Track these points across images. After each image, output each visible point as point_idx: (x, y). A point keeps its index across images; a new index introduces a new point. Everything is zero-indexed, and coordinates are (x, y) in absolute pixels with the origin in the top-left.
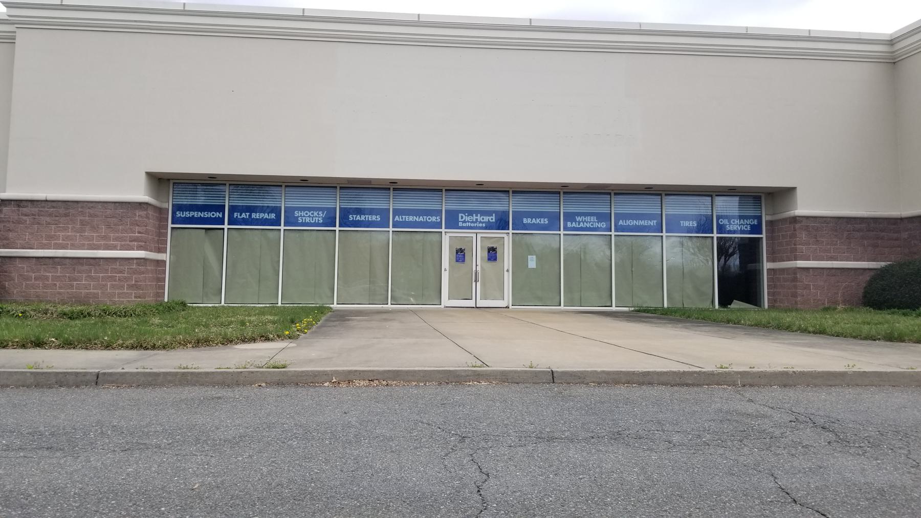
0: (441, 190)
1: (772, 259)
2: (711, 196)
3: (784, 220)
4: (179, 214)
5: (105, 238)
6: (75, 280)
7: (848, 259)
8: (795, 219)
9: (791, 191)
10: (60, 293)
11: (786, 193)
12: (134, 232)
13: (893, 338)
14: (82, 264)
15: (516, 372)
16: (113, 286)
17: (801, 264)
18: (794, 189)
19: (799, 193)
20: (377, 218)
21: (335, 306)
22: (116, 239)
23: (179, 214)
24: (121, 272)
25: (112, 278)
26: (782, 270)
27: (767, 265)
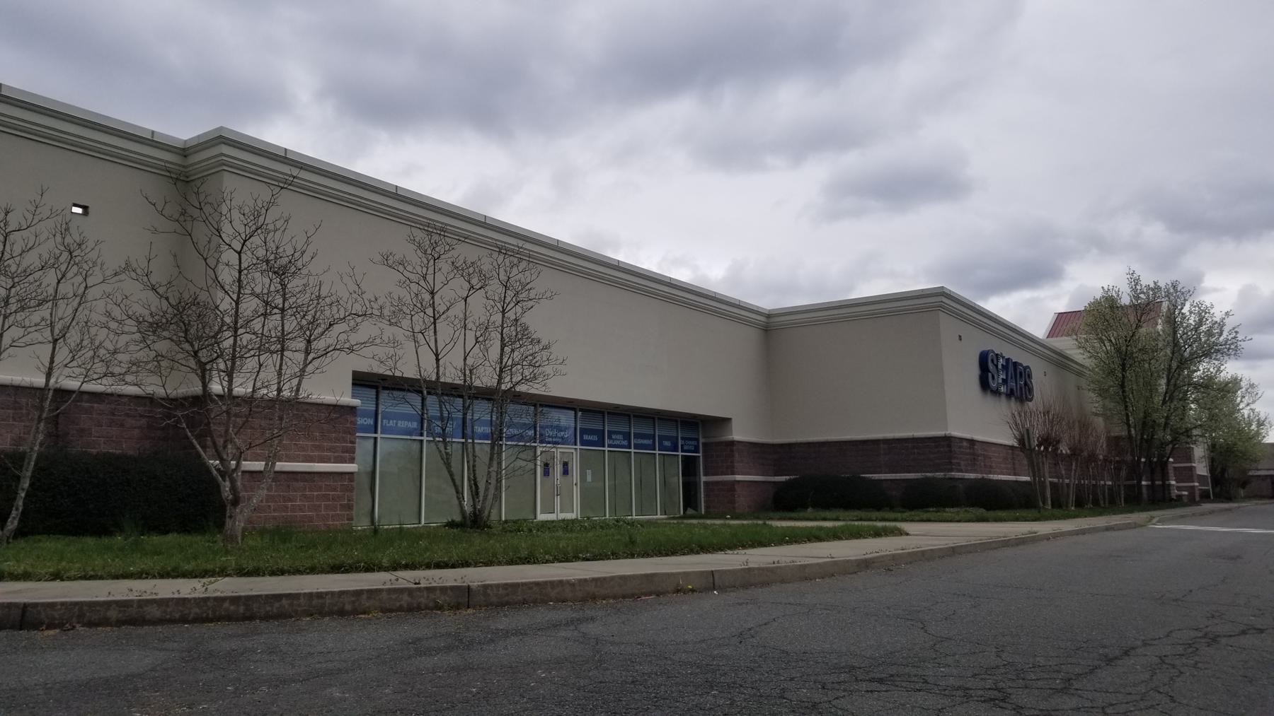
0: (603, 413)
1: (705, 475)
2: (376, 387)
3: (721, 443)
4: (586, 437)
5: (318, 448)
6: (290, 500)
7: (881, 481)
8: (732, 443)
9: (727, 420)
10: (275, 518)
11: (723, 422)
12: (345, 441)
13: (1017, 520)
14: (297, 480)
15: (52, 605)
16: (327, 507)
17: (739, 477)
18: (729, 420)
19: (734, 424)
20: (595, 438)
21: (542, 517)
22: (329, 450)
23: (586, 437)
24: (335, 490)
25: (326, 497)
26: (717, 483)
27: (703, 479)
